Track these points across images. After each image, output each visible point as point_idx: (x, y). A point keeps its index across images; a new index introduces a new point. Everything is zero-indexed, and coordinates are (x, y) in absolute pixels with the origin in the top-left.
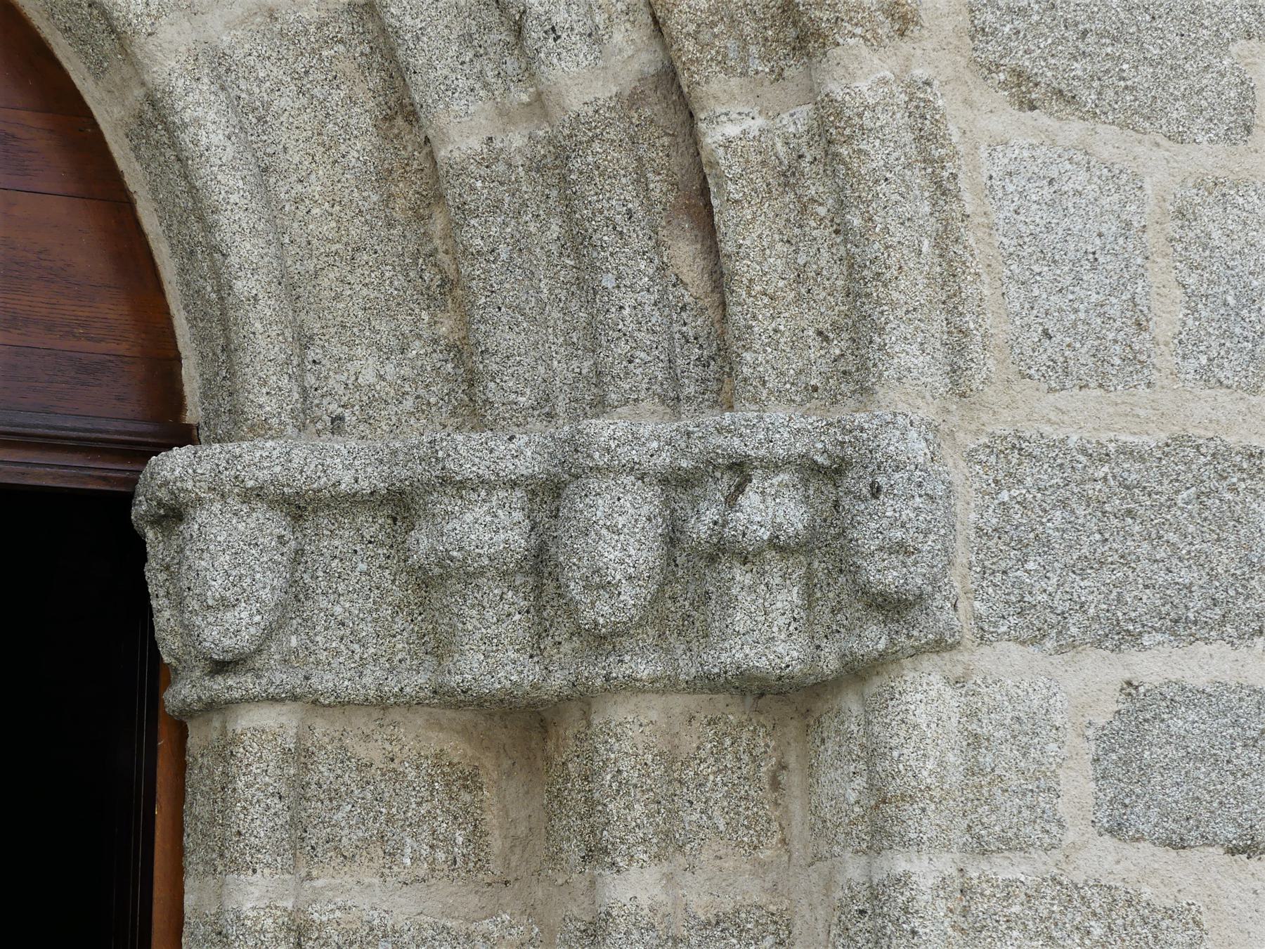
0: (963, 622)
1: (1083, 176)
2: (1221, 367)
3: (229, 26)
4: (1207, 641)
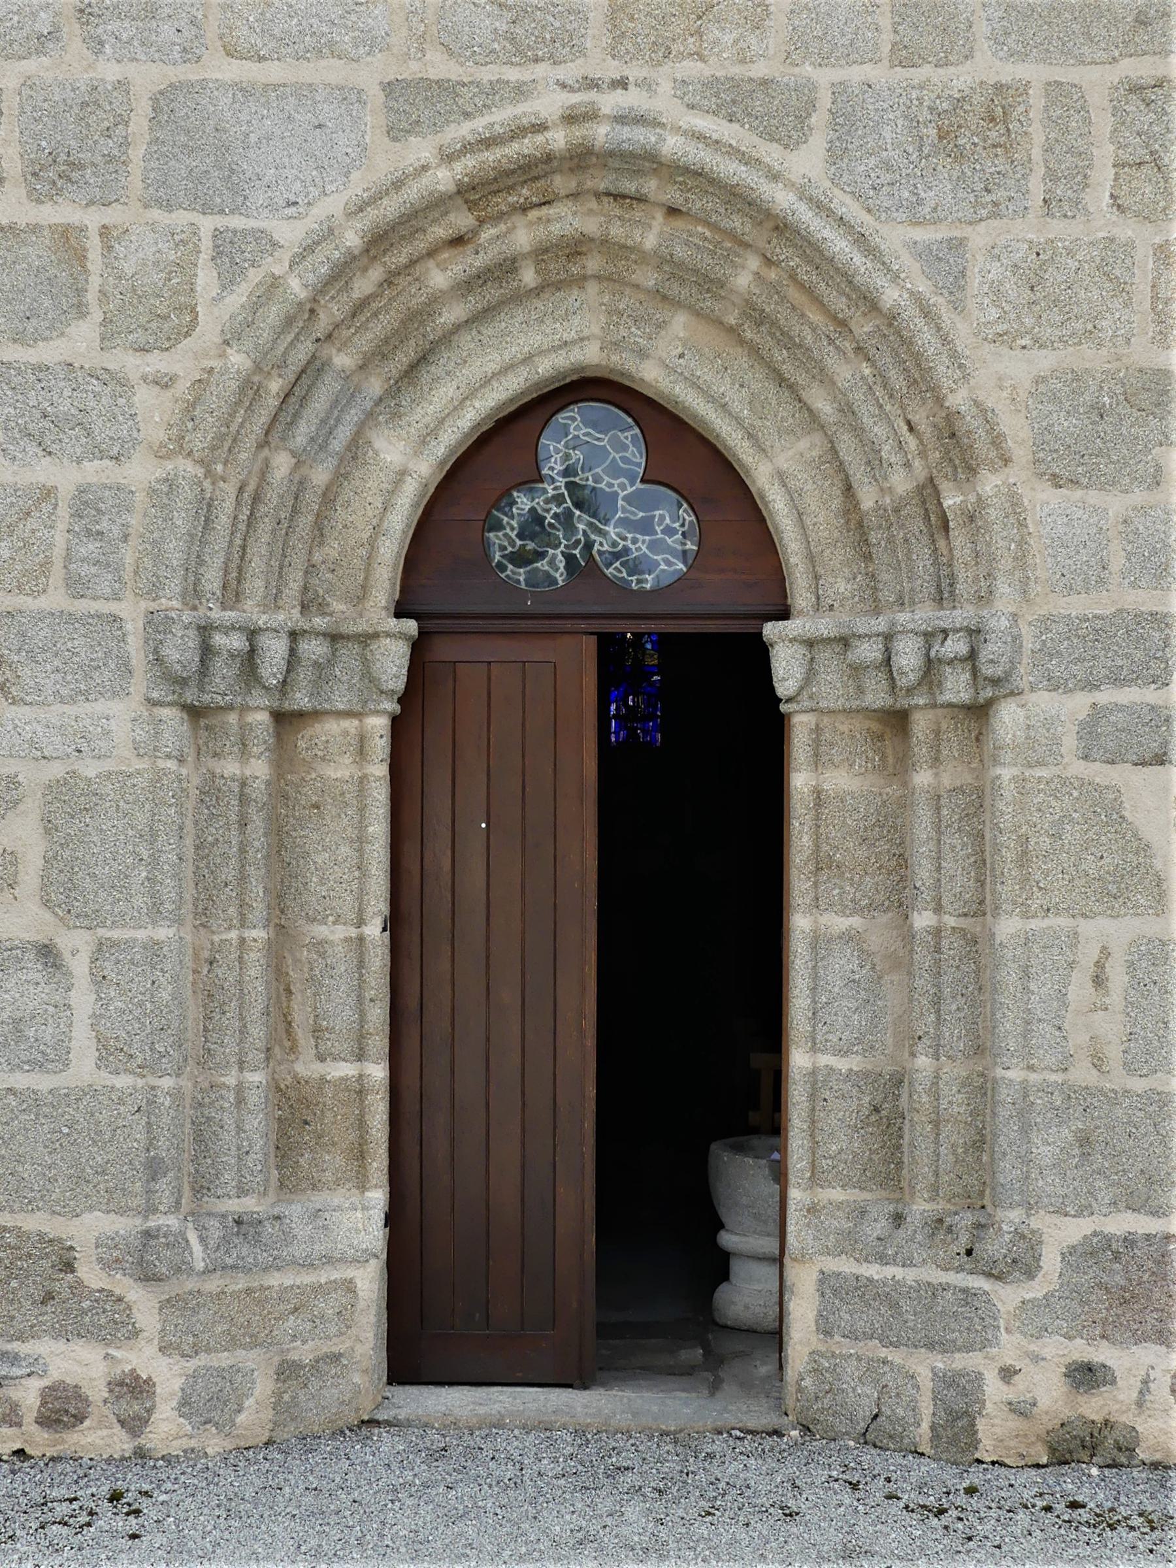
0: (1023, 684)
1: (1081, 512)
2: (1140, 581)
3: (787, 460)
4: (1129, 686)
